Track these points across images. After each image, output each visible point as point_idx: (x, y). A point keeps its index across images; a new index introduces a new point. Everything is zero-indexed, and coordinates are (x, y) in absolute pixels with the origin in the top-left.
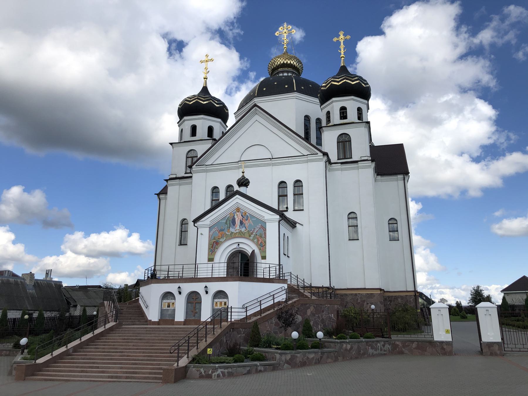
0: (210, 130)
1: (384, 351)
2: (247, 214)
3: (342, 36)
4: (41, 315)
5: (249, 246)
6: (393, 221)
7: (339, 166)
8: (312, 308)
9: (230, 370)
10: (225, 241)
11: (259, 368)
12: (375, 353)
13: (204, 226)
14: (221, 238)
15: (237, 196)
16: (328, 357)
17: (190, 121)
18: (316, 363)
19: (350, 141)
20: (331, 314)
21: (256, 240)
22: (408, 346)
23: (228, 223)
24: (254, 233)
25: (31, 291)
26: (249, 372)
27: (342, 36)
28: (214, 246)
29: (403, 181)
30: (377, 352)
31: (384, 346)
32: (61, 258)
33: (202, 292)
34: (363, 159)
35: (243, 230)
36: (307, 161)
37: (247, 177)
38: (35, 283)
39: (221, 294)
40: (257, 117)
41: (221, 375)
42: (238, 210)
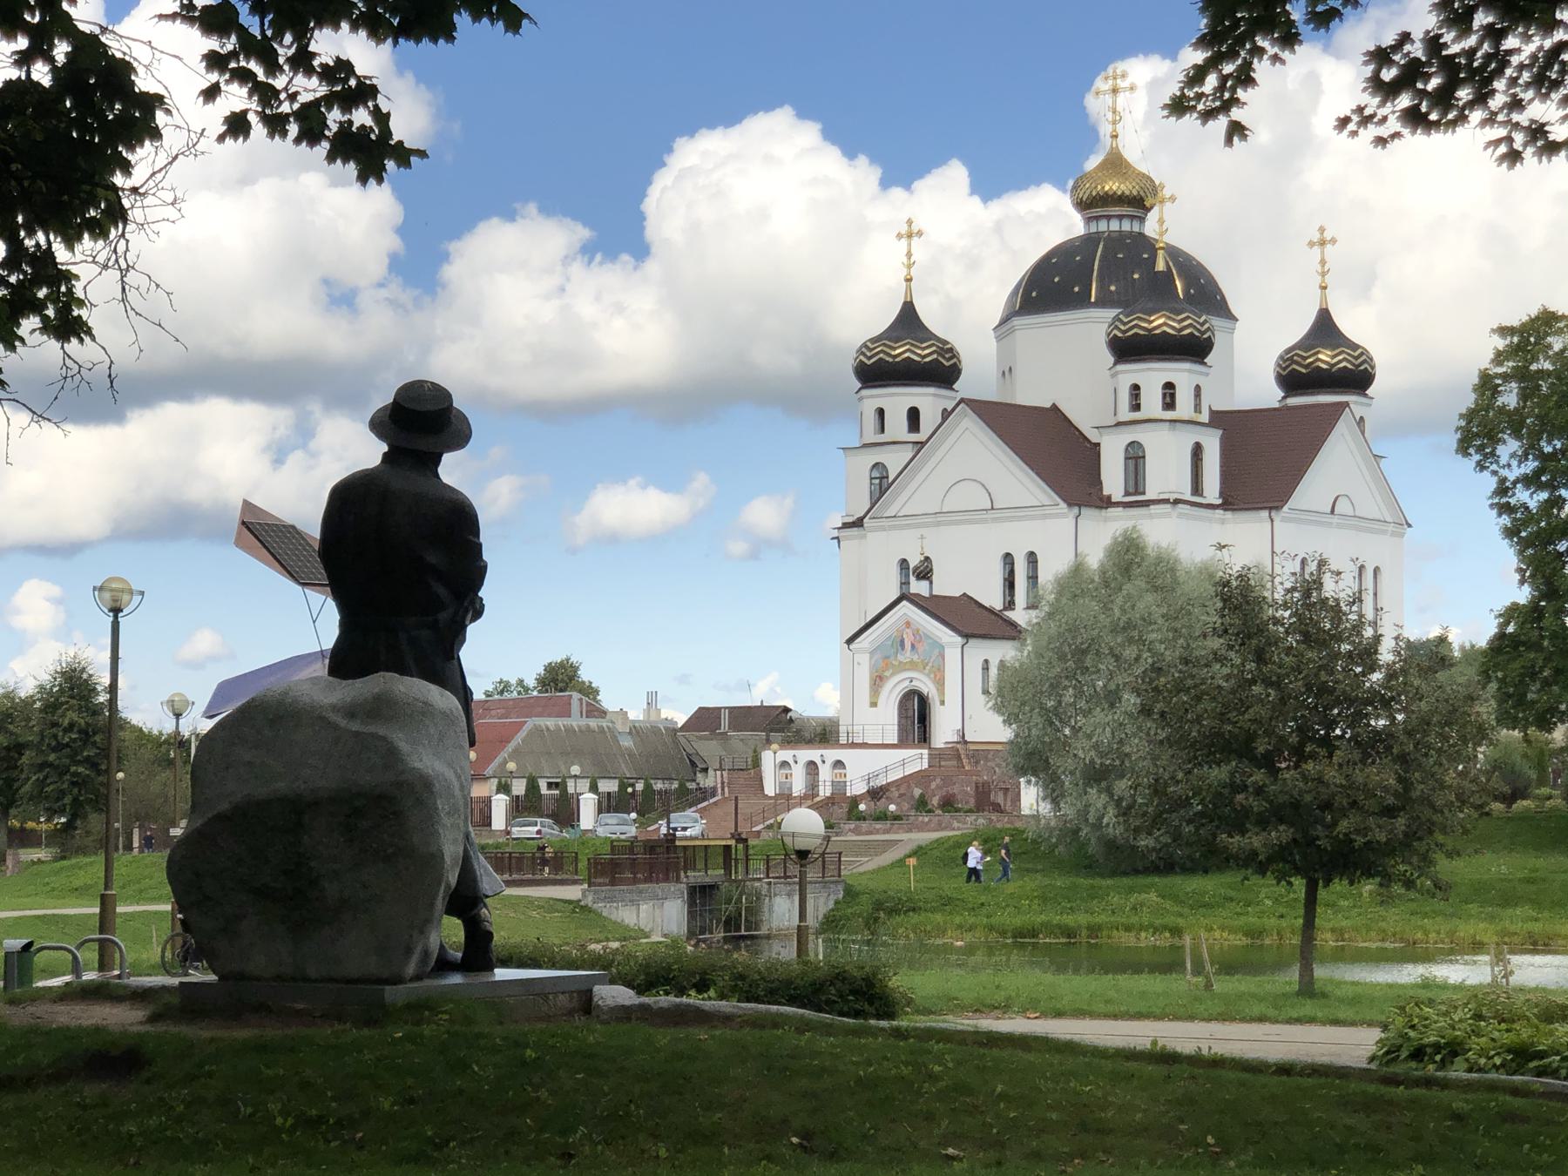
0: (914, 416)
4: (648, 787)
5: (926, 686)
10: (893, 674)
25: (627, 743)
28: (877, 681)
33: (819, 762)
35: (915, 658)
36: (1045, 517)
39: (839, 764)
42: (908, 624)
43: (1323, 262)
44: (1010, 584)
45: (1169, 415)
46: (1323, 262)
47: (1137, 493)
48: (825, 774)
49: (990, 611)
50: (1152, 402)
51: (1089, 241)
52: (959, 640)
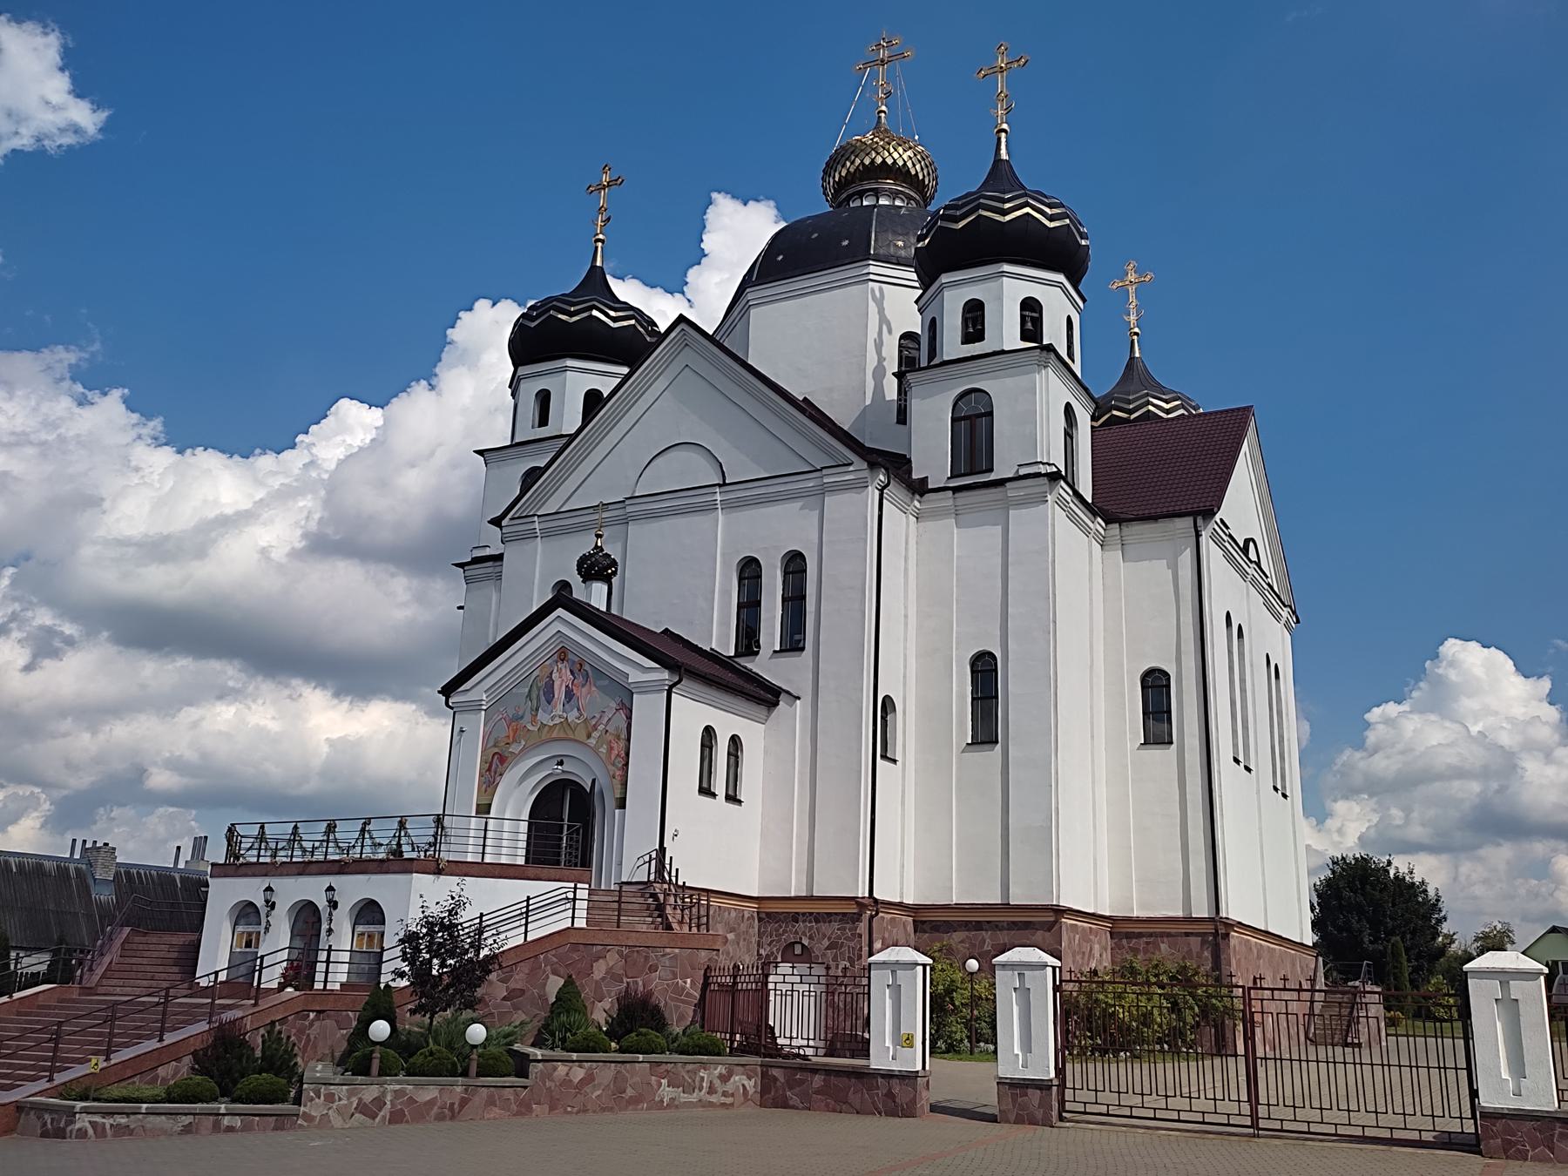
1: (725, 1094)
2: (587, 667)
3: (1132, 277)
5: (586, 770)
6: (1155, 685)
8: (612, 958)
9: (123, 1120)
10: (525, 752)
11: (226, 1121)
12: (684, 1098)
13: (474, 707)
14: (515, 741)
16: (491, 1102)
18: (440, 1117)
20: (684, 978)
21: (603, 750)
22: (802, 1082)
23: (534, 696)
24: (601, 727)
26: (187, 1130)
27: (1132, 277)
28: (495, 765)
30: (694, 1098)
31: (725, 1079)
33: (322, 903)
34: (1023, 471)
35: (572, 716)
38: (117, 874)
40: (687, 356)
41: (91, 1131)
44: (749, 607)
48: (342, 938)
49: (713, 656)
50: (1006, 331)
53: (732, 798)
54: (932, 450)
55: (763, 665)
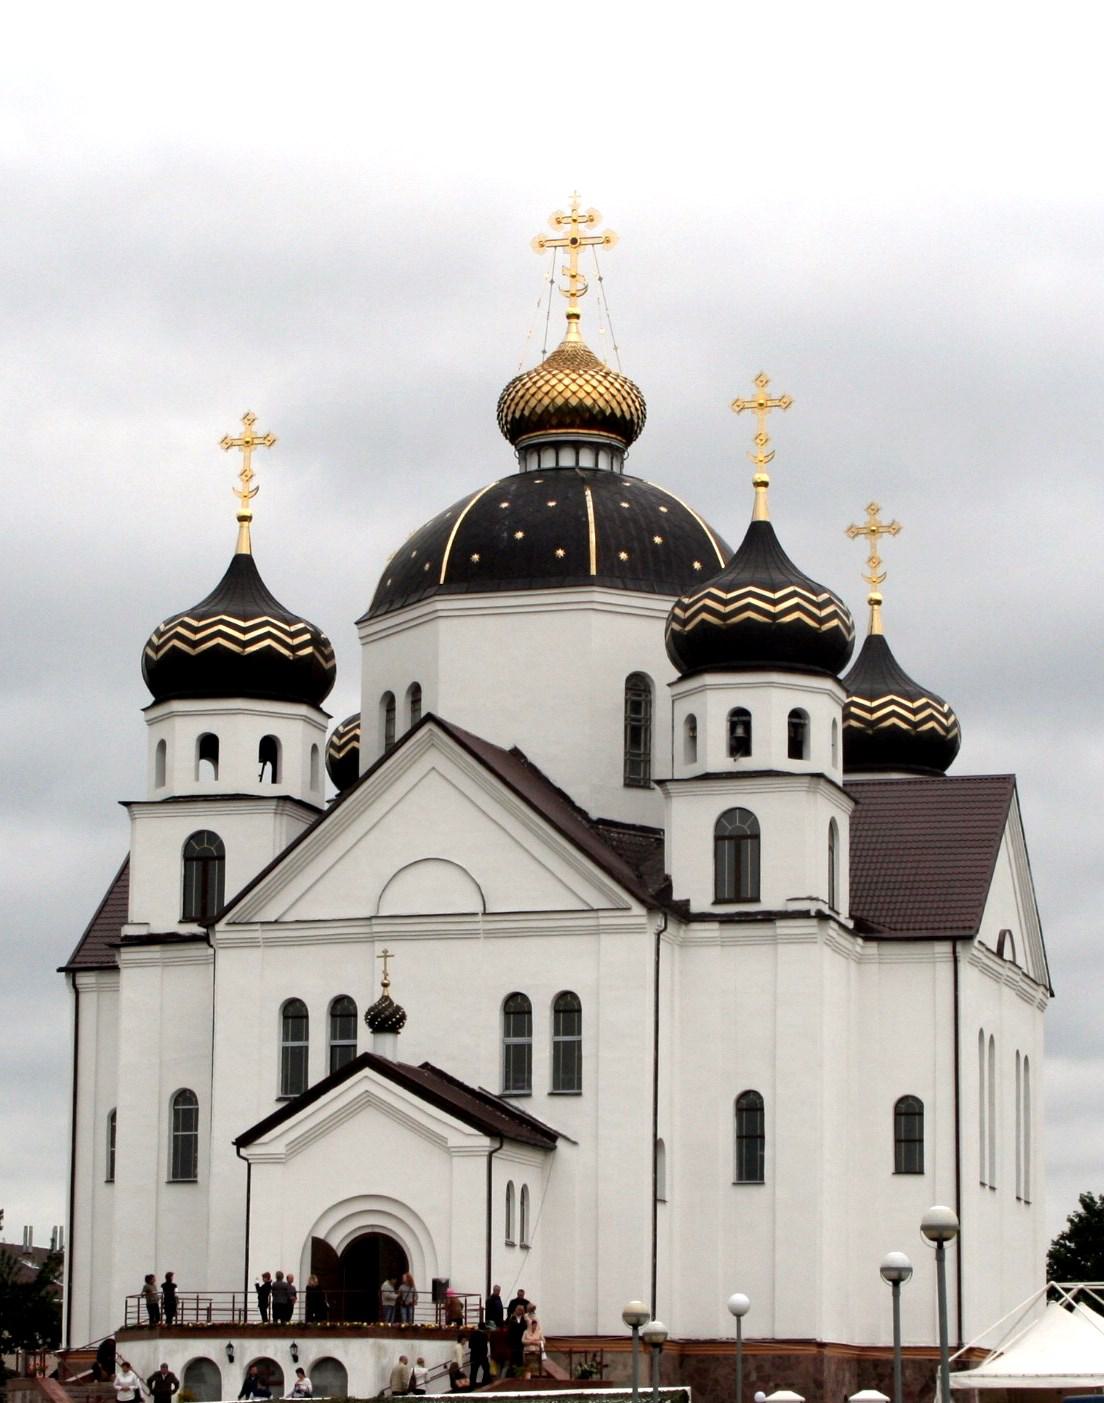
6: (908, 1113)
7: (711, 930)
15: (367, 1072)
17: (190, 719)
19: (756, 837)
29: (950, 966)
32: (296, 1284)
36: (597, 931)
37: (397, 1001)
40: (433, 758)
43: (246, 475)
45: (795, 766)
46: (246, 475)
47: (738, 899)
49: (481, 1097)
50: (769, 746)
51: (524, 477)
52: (484, 1142)
53: (525, 1247)
54: (691, 871)
55: (540, 1105)
